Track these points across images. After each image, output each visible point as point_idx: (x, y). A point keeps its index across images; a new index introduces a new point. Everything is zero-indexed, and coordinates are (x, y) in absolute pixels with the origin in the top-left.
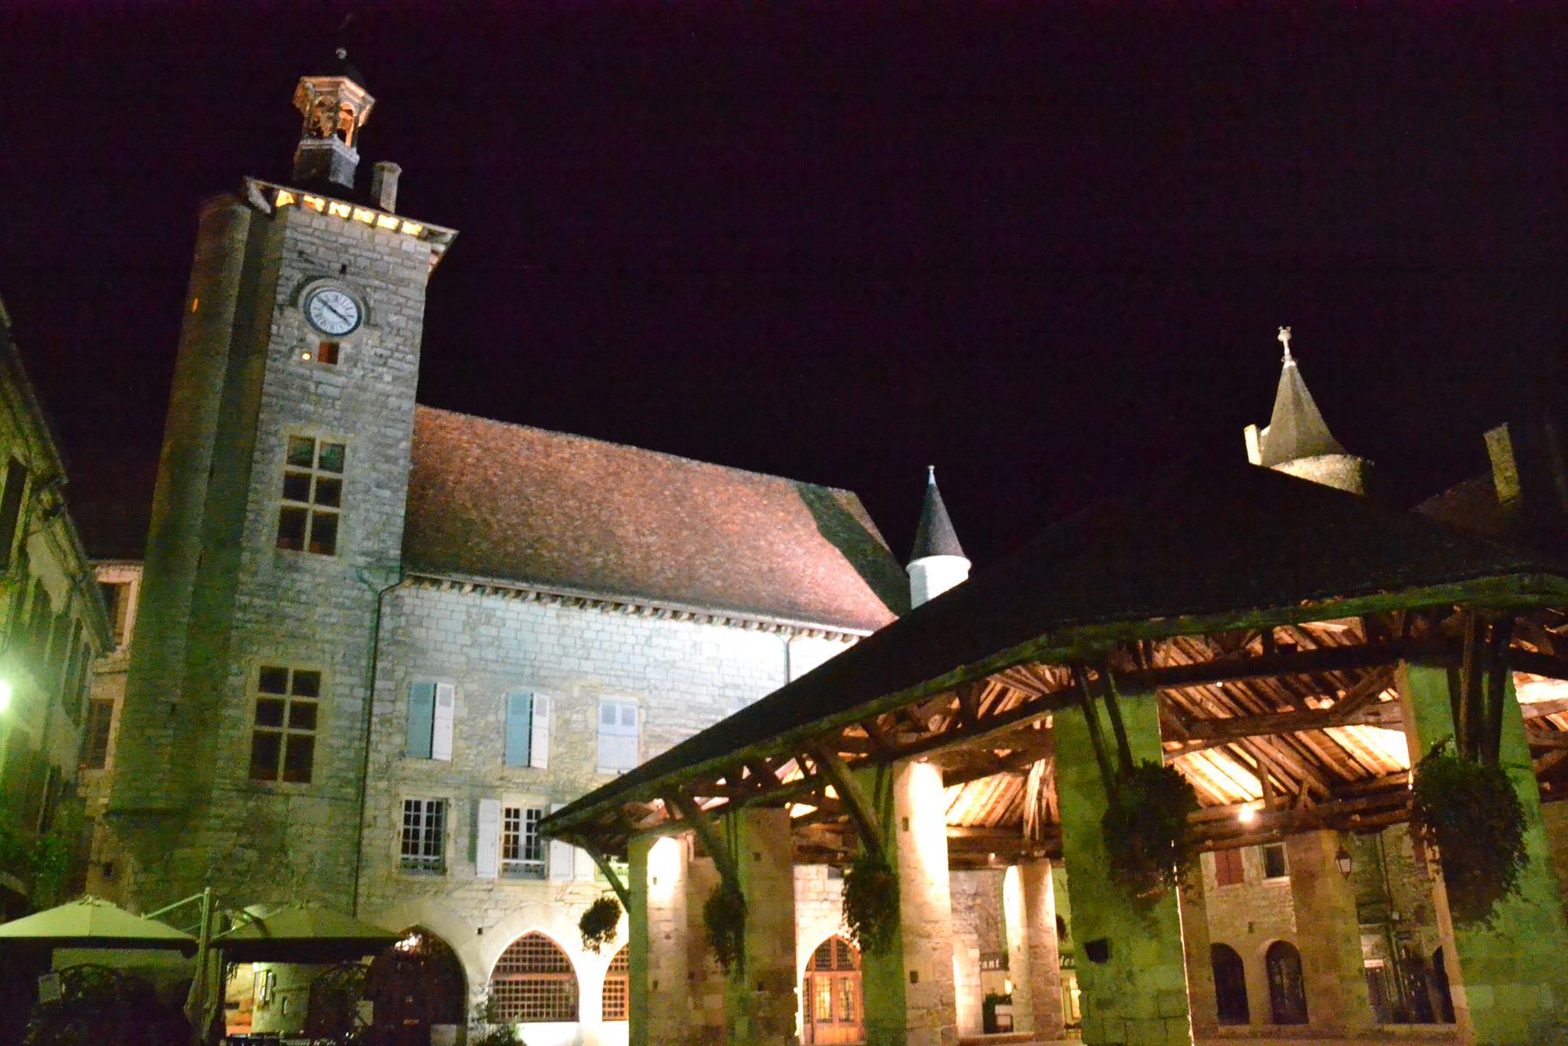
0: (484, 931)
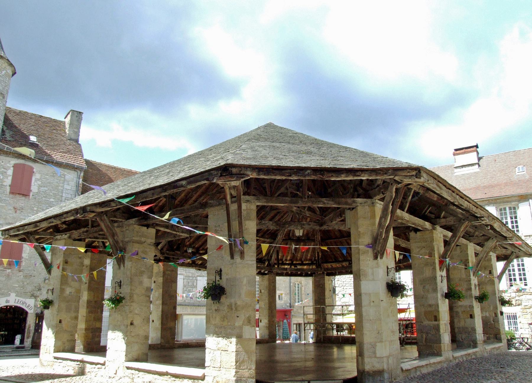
0: (238, 316)
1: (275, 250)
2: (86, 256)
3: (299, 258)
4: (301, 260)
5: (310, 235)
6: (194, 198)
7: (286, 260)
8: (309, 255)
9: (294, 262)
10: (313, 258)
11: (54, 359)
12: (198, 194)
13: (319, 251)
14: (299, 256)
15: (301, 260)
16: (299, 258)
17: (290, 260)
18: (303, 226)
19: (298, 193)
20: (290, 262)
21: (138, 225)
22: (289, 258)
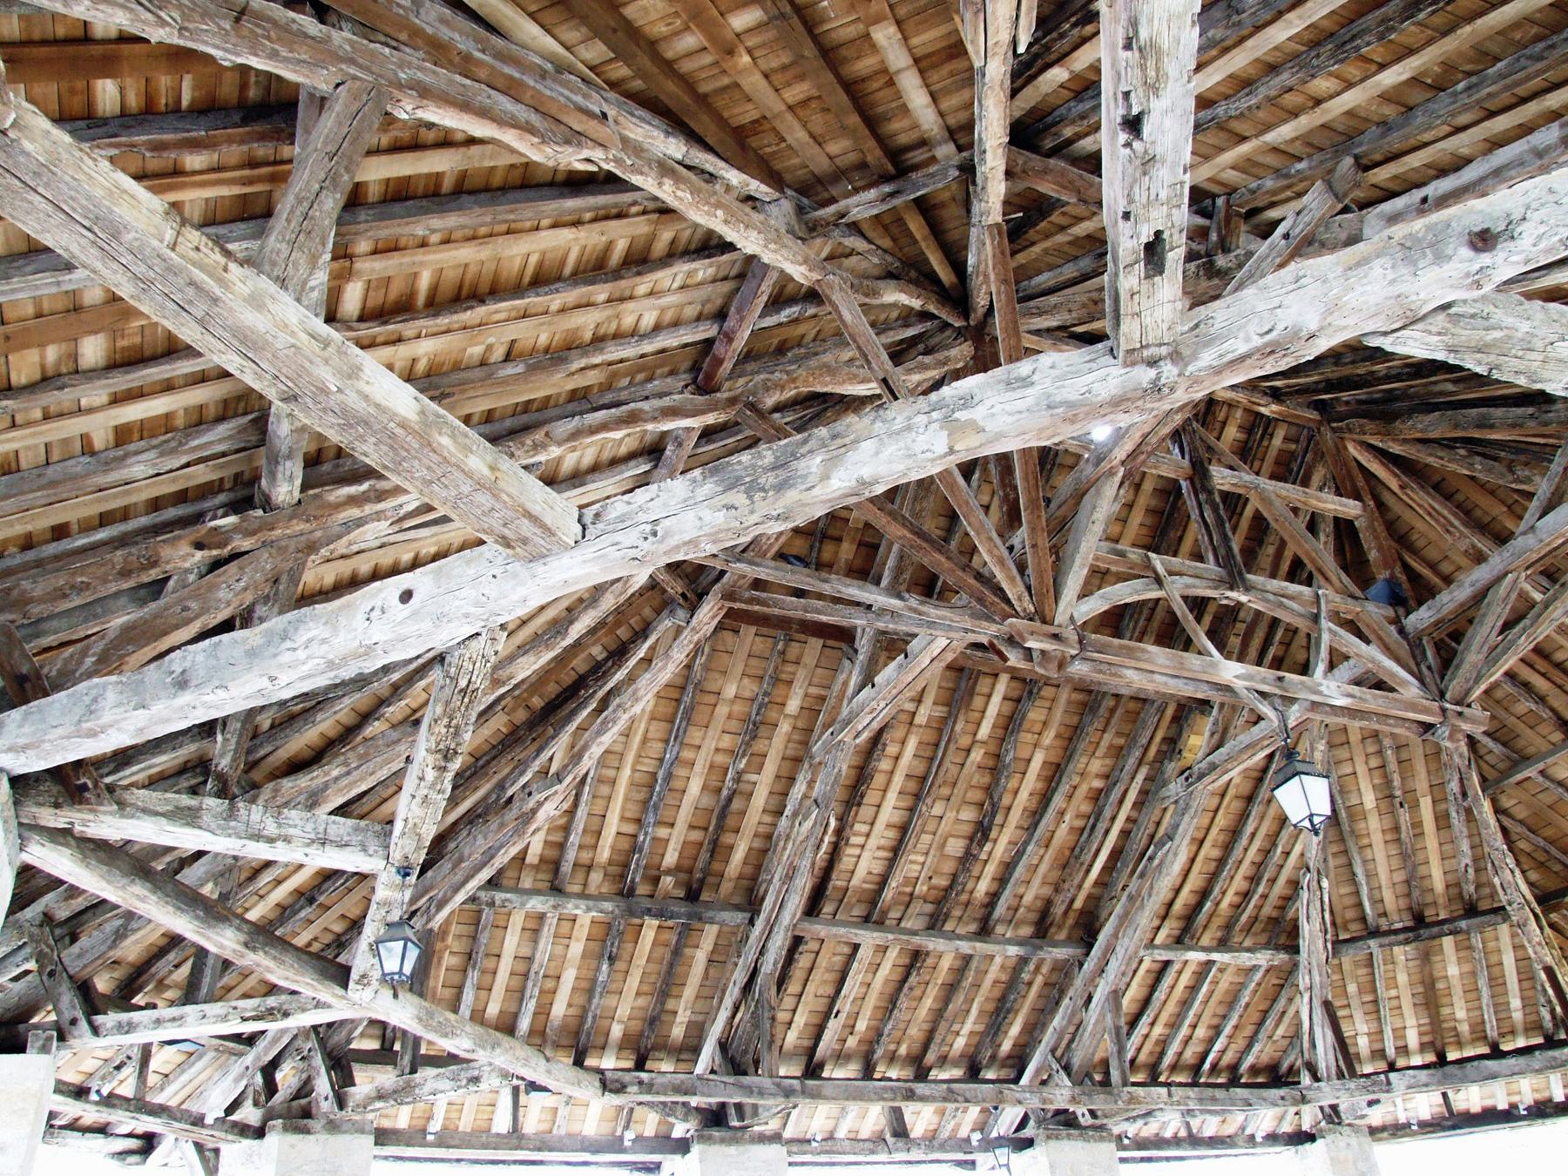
1: (1317, 1003)
2: (260, 1155)
3: (1464, 1028)
4: (1479, 1035)
5: (1472, 888)
6: (760, 798)
7: (1403, 1050)
8: (1516, 1003)
9: (1452, 1056)
10: (1545, 1014)
11: (57, 1091)
12: (771, 767)
13: (1549, 960)
14: (1461, 1014)
15: (1479, 1035)
16: (1464, 1028)
17: (1423, 1048)
18: (961, 415)
19: (1244, 598)
20: (1431, 1057)
21: (281, 613)
22: (1413, 1039)
